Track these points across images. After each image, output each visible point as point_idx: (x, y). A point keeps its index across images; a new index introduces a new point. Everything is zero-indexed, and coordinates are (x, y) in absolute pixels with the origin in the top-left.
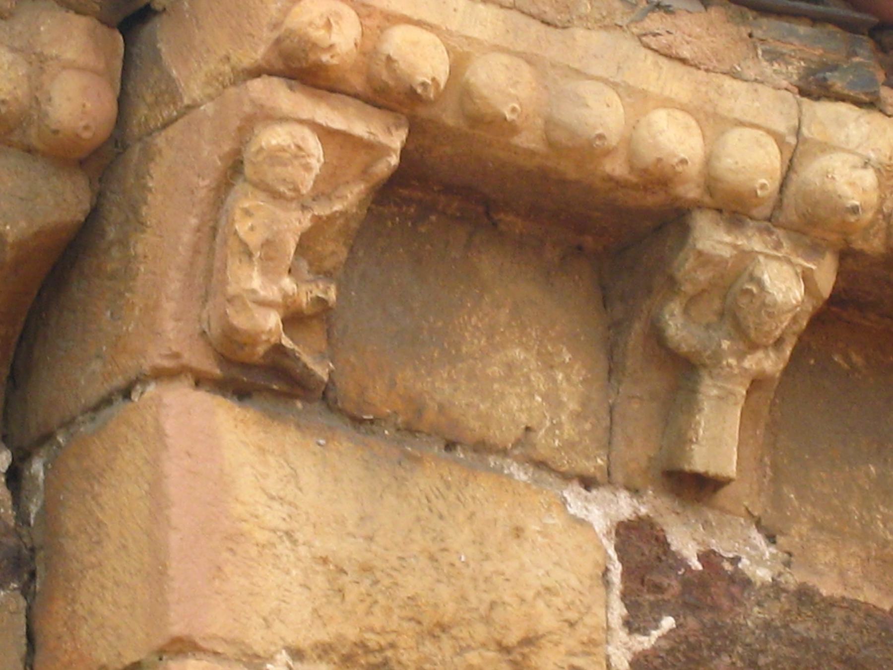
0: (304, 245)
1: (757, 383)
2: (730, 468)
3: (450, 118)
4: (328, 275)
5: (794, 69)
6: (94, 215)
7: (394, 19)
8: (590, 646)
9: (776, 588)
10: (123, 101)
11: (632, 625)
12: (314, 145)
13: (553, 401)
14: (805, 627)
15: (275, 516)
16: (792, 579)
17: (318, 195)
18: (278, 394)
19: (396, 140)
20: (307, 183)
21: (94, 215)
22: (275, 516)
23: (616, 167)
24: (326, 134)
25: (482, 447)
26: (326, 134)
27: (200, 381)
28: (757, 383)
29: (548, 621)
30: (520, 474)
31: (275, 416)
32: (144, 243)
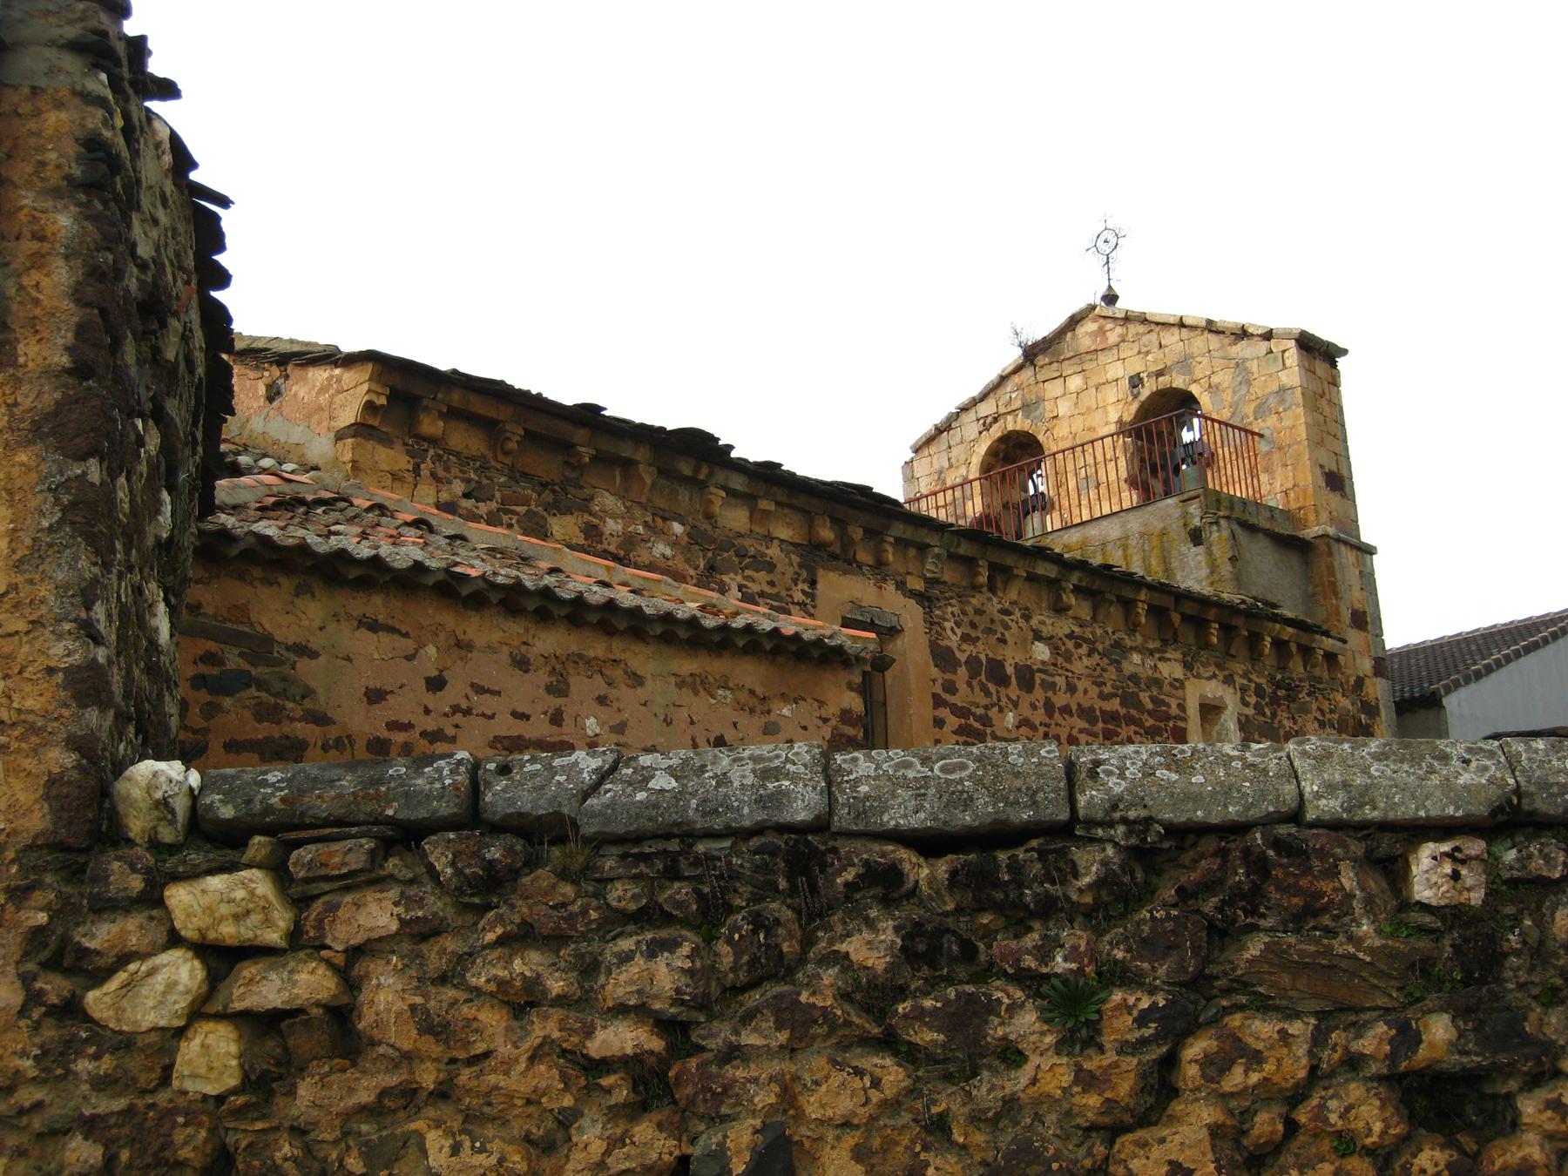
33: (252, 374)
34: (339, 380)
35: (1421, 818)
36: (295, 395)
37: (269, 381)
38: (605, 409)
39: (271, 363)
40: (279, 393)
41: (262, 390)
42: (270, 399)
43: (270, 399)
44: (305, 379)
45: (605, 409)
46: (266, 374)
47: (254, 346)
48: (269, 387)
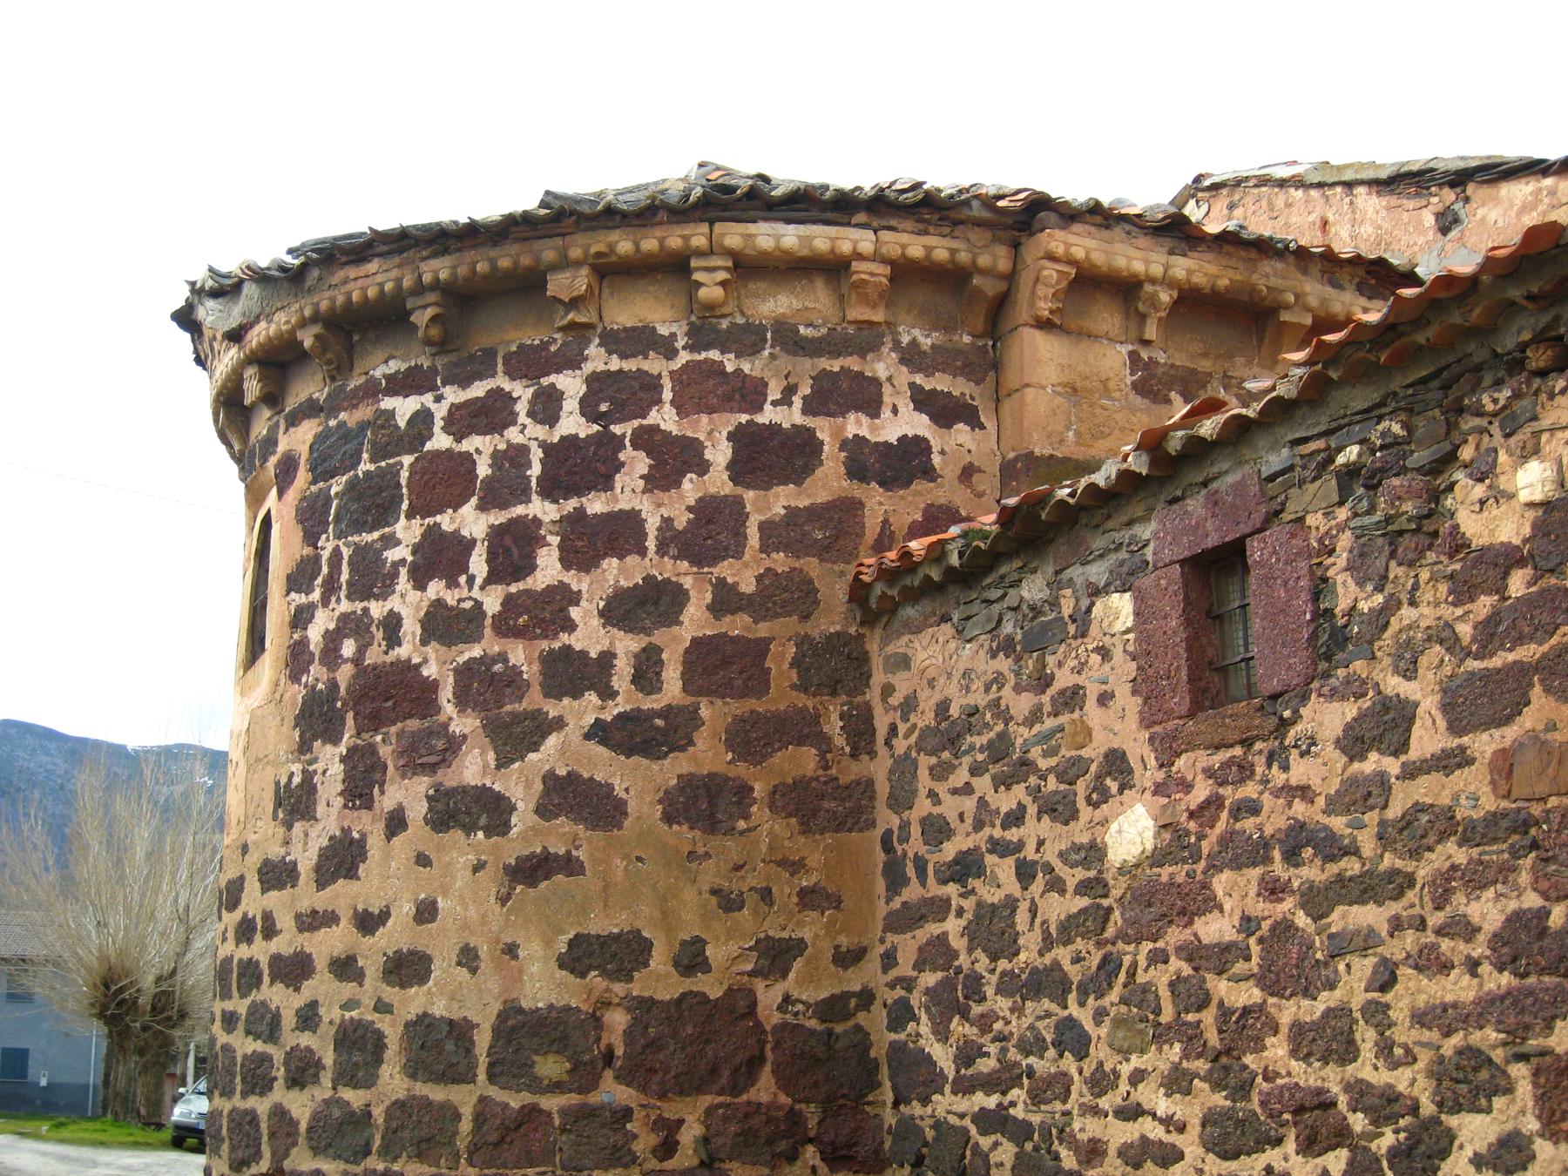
0: (1054, 295)
1: (1160, 319)
2: (1154, 337)
3: (1086, 265)
4: (1059, 301)
5: (1166, 249)
6: (1009, 289)
7: (1072, 245)
8: (1121, 380)
9: (1166, 364)
10: (1015, 265)
11: (1131, 375)
12: (1055, 274)
13: (1113, 325)
14: (1173, 372)
15: (1049, 355)
16: (1169, 362)
17: (1057, 284)
18: (1002, 197)
19: (1074, 271)
20: (1053, 282)
21: (1009, 289)
22: (1049, 355)
23: (1125, 274)
24: (1057, 271)
25: (1096, 336)
26: (1057, 271)
27: (1032, 326)
28: (1160, 319)
29: (1111, 375)
30: (1106, 342)
31: (1048, 333)
32: (1019, 296)
33: (1410, 204)
34: (1552, 192)
35: (650, 255)
36: (1483, 219)
37: (1440, 208)
38: (925, 183)
39: (1441, 185)
40: (1456, 221)
41: (1429, 219)
42: (1444, 230)
43: (1444, 230)
44: (1497, 201)
45: (925, 183)
46: (1434, 200)
47: (1402, 170)
48: (1439, 216)
